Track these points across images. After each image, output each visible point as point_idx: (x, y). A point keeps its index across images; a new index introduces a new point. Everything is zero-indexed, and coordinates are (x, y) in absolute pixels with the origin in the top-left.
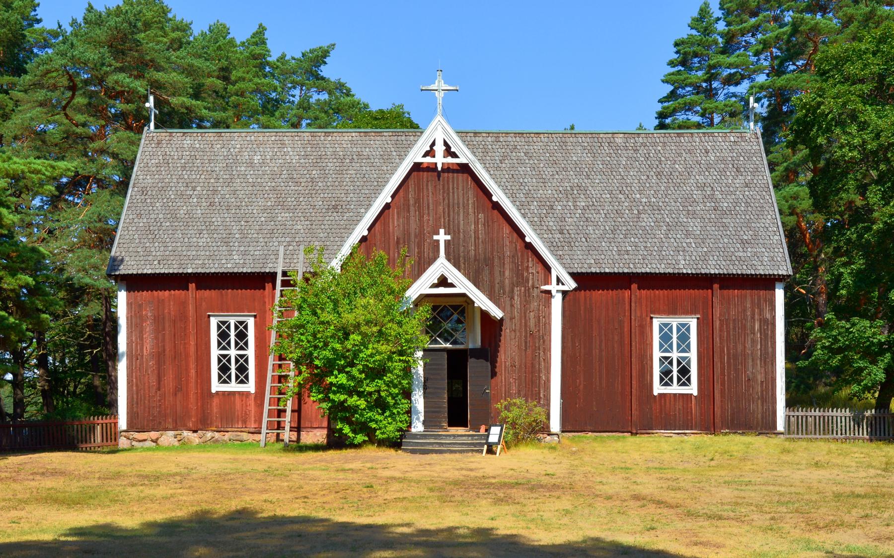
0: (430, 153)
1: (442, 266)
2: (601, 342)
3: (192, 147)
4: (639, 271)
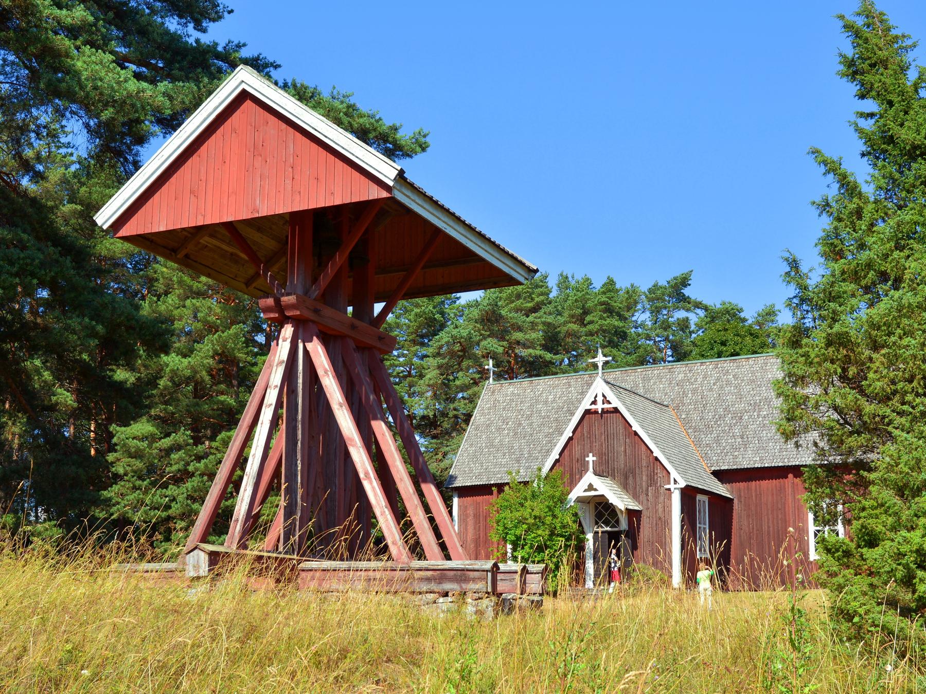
0: (594, 402)
1: (589, 478)
2: (768, 520)
3: (513, 393)
4: (790, 464)
